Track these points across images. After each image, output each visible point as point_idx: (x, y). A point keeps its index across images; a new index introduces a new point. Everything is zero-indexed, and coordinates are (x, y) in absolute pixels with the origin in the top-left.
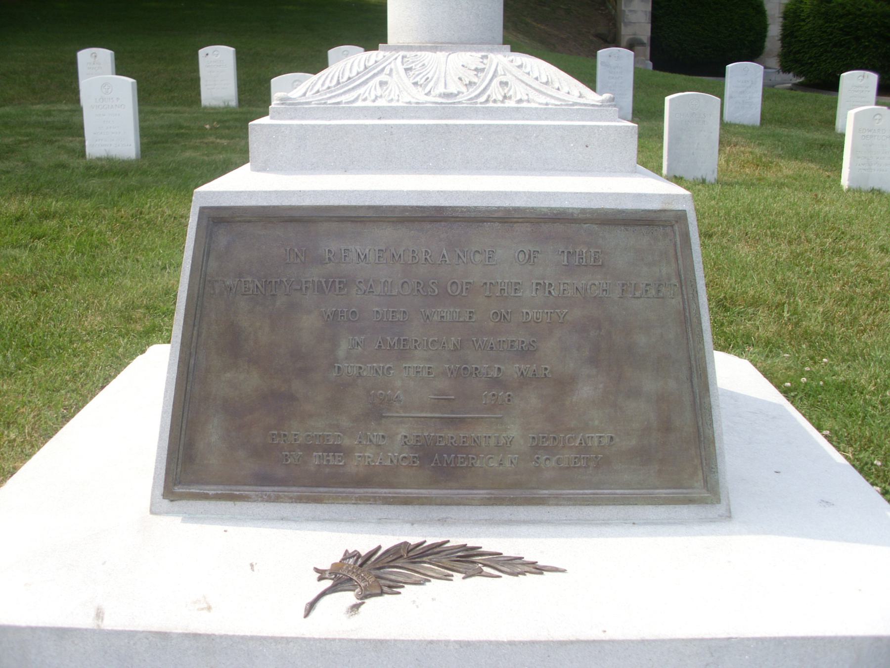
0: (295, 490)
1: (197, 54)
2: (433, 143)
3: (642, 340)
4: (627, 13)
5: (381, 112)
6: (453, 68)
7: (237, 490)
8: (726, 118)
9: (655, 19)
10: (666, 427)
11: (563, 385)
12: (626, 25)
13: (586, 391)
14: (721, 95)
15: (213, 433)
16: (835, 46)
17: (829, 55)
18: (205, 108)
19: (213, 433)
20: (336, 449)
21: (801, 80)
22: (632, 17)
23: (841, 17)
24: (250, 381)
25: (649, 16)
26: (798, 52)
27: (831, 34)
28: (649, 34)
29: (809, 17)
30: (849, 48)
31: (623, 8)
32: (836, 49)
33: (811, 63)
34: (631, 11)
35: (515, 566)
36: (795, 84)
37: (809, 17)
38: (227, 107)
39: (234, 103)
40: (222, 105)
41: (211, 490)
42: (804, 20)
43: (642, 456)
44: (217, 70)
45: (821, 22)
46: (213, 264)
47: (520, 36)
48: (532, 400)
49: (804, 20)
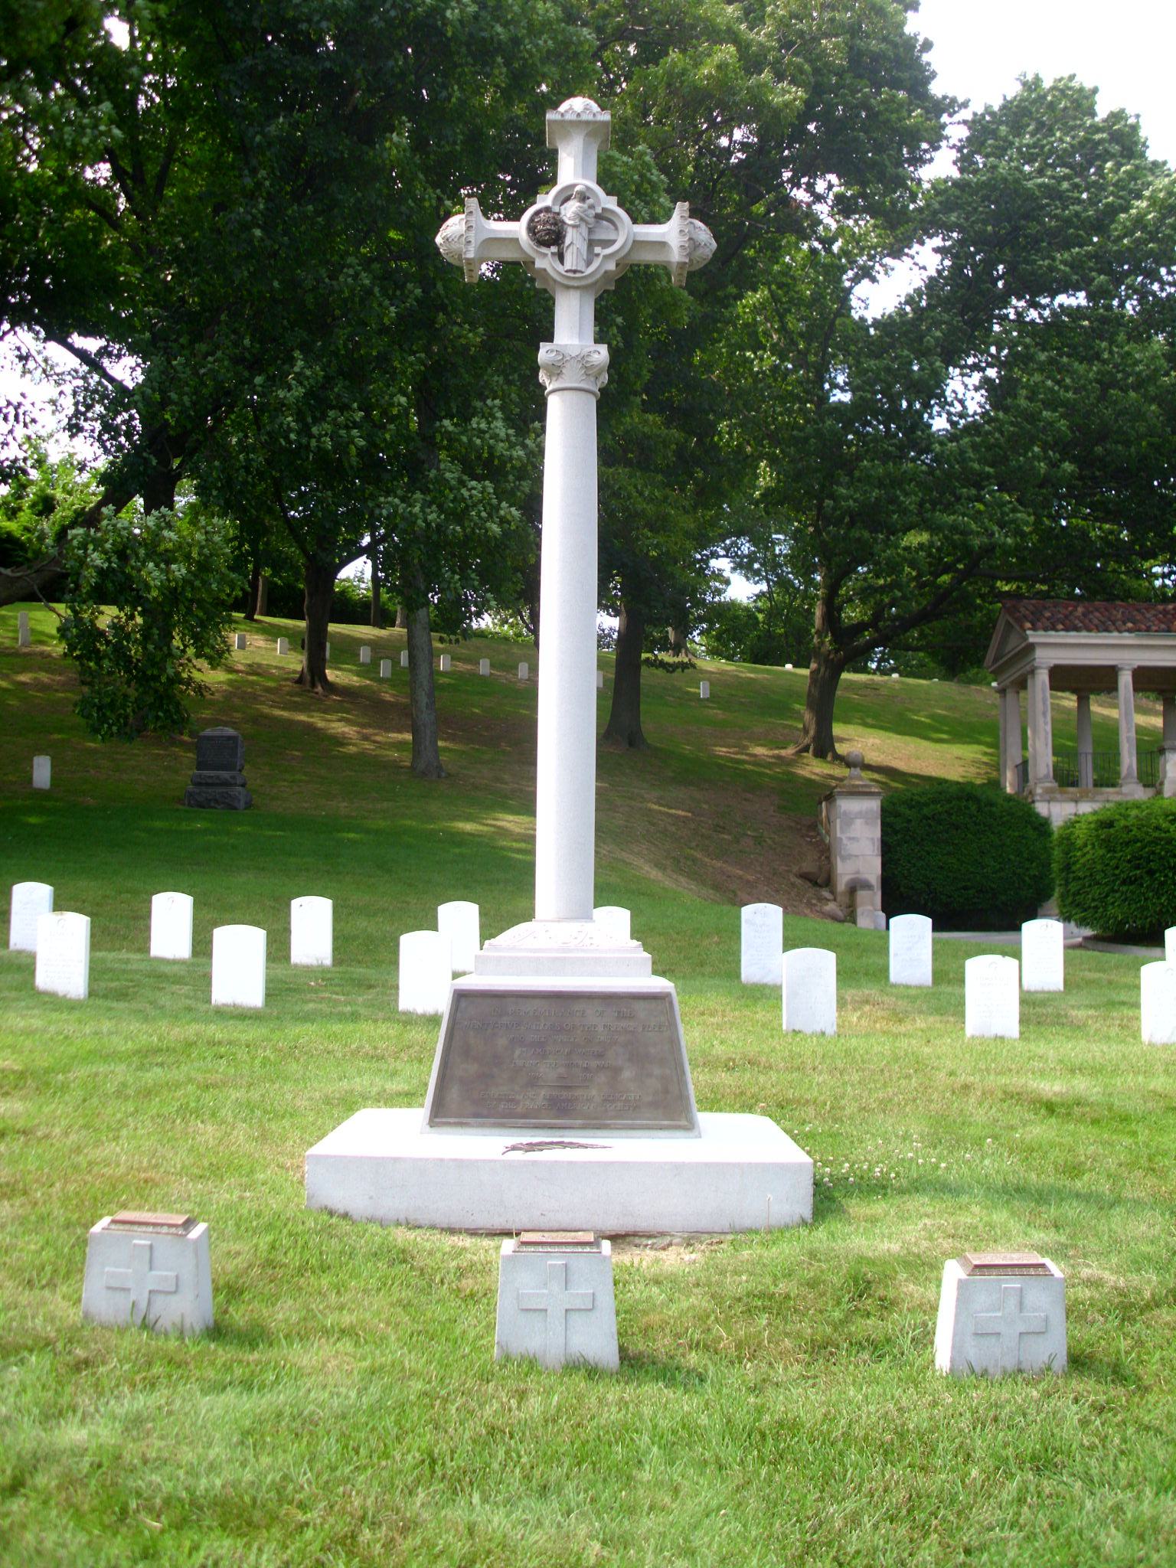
0: (492, 1120)
1: (289, 906)
2: (558, 964)
3: (652, 1050)
4: (845, 841)
5: (531, 951)
6: (571, 932)
7: (465, 1120)
8: (1025, 987)
9: (888, 850)
10: (666, 1091)
11: (616, 1071)
12: (843, 859)
13: (627, 1074)
14: (1017, 954)
15: (454, 1093)
16: (1124, 883)
17: (1117, 895)
18: (296, 965)
19: (454, 1093)
20: (512, 1100)
21: (1088, 932)
22: (851, 848)
23: (1127, 844)
24: (473, 1068)
25: (878, 844)
26: (1078, 893)
27: (1117, 868)
28: (879, 871)
29: (1085, 845)
30: (1141, 885)
31: (839, 835)
32: (1124, 888)
33: (1096, 907)
34: (850, 839)
35: (592, 1147)
36: (1086, 939)
37: (1085, 845)
38: (321, 965)
39: (328, 961)
40: (315, 963)
41: (451, 1120)
42: (1080, 849)
43: (654, 1105)
44: (171, 917)
45: (1101, 852)
46: (459, 1015)
47: (682, 879)
48: (602, 1078)
49: (1080, 849)
